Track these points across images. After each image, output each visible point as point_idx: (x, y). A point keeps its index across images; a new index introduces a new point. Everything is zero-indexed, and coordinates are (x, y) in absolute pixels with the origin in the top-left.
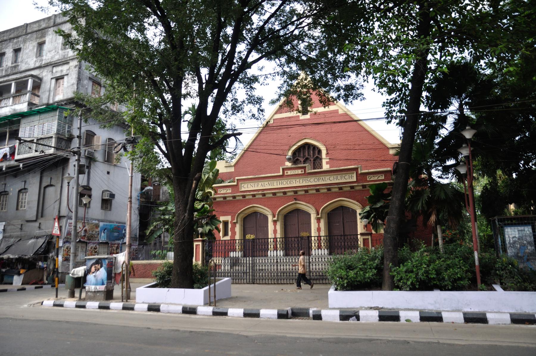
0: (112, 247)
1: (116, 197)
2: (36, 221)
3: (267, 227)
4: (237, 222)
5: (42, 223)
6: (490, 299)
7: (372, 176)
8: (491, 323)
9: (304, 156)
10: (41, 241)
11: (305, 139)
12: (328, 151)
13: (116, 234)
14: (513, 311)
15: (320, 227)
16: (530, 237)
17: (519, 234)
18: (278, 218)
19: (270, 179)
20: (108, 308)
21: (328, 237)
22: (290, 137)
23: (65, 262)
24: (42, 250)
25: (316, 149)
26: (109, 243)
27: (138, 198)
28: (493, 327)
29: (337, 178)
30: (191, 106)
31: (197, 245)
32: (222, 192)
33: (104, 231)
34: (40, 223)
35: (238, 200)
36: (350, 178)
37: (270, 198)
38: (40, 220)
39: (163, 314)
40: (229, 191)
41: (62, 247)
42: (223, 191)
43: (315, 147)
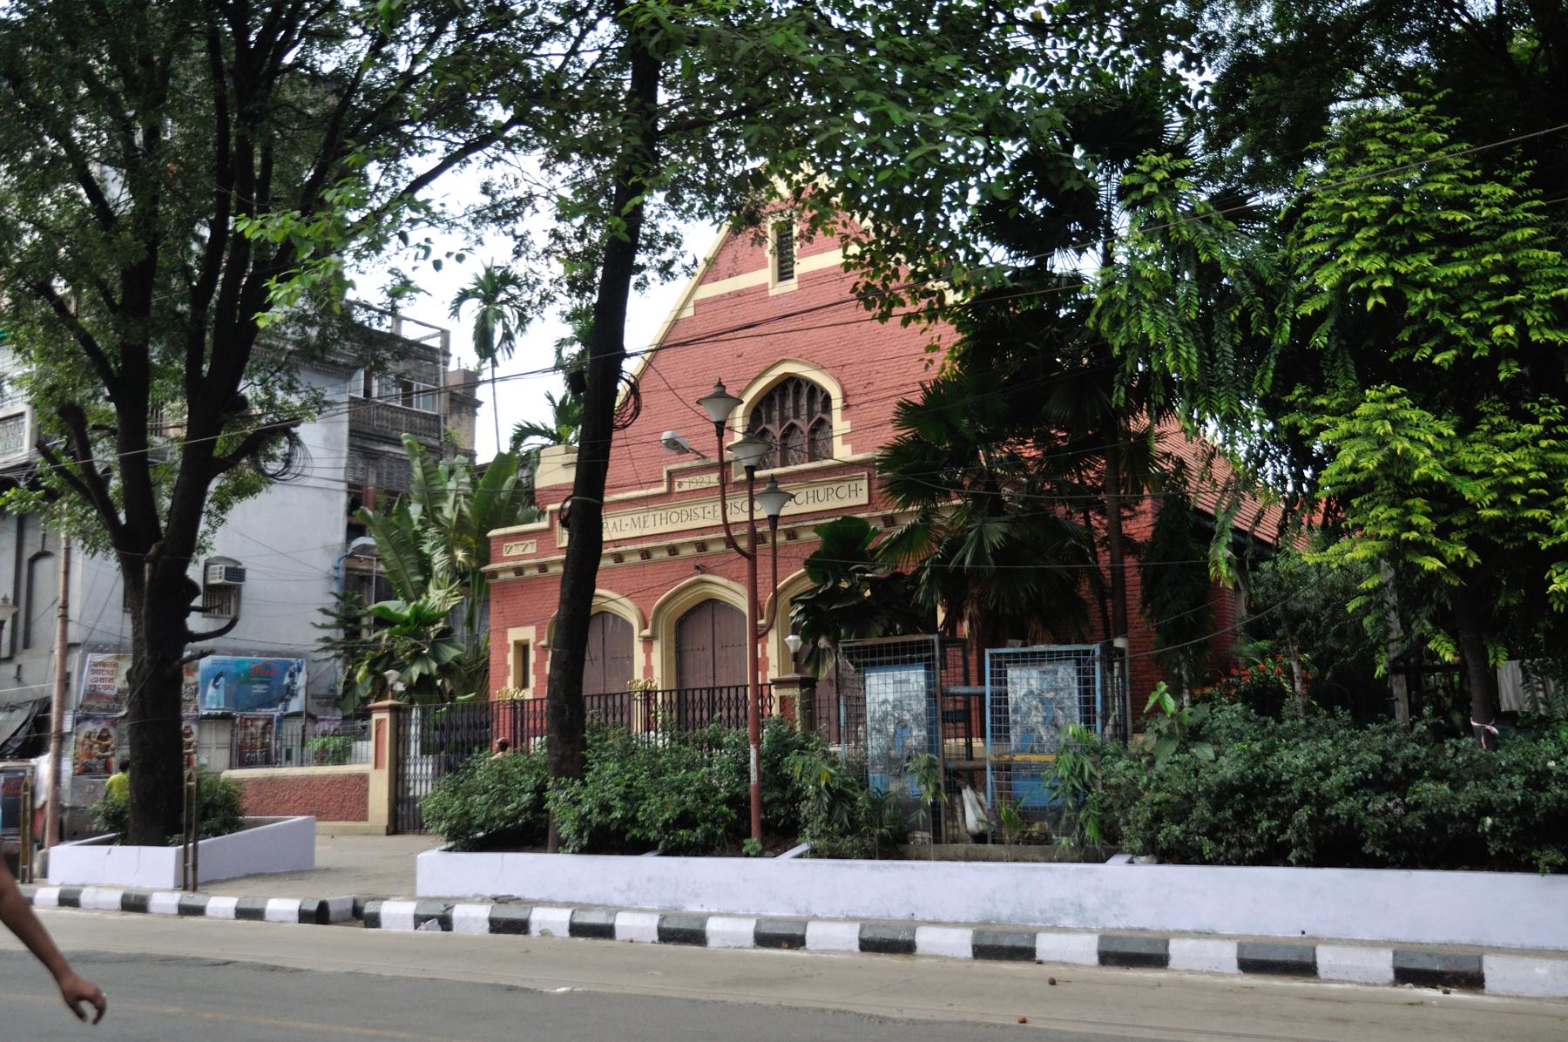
0: (246, 727)
1: (248, 575)
2: (10, 659)
3: (631, 658)
4: (770, 626)
5: (24, 667)
6: (745, 880)
7: (512, 544)
8: (713, 943)
9: (783, 419)
10: (19, 717)
11: (783, 361)
12: (851, 401)
13: (259, 689)
14: (1403, 934)
15: (768, 655)
16: (919, 702)
17: (1042, 680)
18: (654, 630)
19: (637, 505)
20: (199, 911)
21: (674, 695)
22: (740, 360)
23: (85, 778)
24: (17, 745)
25: (819, 393)
26: (235, 718)
27: (333, 572)
28: (389, 935)
29: (816, 498)
30: (482, 274)
31: (379, 722)
32: (514, 553)
33: (216, 680)
34: (19, 667)
35: (531, 579)
36: (853, 494)
37: (635, 565)
38: (23, 658)
39: (1493, 1000)
40: (531, 547)
41: (70, 733)
42: (515, 549)
43: (814, 389)
